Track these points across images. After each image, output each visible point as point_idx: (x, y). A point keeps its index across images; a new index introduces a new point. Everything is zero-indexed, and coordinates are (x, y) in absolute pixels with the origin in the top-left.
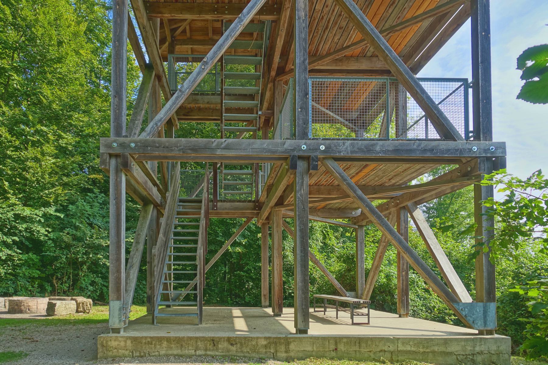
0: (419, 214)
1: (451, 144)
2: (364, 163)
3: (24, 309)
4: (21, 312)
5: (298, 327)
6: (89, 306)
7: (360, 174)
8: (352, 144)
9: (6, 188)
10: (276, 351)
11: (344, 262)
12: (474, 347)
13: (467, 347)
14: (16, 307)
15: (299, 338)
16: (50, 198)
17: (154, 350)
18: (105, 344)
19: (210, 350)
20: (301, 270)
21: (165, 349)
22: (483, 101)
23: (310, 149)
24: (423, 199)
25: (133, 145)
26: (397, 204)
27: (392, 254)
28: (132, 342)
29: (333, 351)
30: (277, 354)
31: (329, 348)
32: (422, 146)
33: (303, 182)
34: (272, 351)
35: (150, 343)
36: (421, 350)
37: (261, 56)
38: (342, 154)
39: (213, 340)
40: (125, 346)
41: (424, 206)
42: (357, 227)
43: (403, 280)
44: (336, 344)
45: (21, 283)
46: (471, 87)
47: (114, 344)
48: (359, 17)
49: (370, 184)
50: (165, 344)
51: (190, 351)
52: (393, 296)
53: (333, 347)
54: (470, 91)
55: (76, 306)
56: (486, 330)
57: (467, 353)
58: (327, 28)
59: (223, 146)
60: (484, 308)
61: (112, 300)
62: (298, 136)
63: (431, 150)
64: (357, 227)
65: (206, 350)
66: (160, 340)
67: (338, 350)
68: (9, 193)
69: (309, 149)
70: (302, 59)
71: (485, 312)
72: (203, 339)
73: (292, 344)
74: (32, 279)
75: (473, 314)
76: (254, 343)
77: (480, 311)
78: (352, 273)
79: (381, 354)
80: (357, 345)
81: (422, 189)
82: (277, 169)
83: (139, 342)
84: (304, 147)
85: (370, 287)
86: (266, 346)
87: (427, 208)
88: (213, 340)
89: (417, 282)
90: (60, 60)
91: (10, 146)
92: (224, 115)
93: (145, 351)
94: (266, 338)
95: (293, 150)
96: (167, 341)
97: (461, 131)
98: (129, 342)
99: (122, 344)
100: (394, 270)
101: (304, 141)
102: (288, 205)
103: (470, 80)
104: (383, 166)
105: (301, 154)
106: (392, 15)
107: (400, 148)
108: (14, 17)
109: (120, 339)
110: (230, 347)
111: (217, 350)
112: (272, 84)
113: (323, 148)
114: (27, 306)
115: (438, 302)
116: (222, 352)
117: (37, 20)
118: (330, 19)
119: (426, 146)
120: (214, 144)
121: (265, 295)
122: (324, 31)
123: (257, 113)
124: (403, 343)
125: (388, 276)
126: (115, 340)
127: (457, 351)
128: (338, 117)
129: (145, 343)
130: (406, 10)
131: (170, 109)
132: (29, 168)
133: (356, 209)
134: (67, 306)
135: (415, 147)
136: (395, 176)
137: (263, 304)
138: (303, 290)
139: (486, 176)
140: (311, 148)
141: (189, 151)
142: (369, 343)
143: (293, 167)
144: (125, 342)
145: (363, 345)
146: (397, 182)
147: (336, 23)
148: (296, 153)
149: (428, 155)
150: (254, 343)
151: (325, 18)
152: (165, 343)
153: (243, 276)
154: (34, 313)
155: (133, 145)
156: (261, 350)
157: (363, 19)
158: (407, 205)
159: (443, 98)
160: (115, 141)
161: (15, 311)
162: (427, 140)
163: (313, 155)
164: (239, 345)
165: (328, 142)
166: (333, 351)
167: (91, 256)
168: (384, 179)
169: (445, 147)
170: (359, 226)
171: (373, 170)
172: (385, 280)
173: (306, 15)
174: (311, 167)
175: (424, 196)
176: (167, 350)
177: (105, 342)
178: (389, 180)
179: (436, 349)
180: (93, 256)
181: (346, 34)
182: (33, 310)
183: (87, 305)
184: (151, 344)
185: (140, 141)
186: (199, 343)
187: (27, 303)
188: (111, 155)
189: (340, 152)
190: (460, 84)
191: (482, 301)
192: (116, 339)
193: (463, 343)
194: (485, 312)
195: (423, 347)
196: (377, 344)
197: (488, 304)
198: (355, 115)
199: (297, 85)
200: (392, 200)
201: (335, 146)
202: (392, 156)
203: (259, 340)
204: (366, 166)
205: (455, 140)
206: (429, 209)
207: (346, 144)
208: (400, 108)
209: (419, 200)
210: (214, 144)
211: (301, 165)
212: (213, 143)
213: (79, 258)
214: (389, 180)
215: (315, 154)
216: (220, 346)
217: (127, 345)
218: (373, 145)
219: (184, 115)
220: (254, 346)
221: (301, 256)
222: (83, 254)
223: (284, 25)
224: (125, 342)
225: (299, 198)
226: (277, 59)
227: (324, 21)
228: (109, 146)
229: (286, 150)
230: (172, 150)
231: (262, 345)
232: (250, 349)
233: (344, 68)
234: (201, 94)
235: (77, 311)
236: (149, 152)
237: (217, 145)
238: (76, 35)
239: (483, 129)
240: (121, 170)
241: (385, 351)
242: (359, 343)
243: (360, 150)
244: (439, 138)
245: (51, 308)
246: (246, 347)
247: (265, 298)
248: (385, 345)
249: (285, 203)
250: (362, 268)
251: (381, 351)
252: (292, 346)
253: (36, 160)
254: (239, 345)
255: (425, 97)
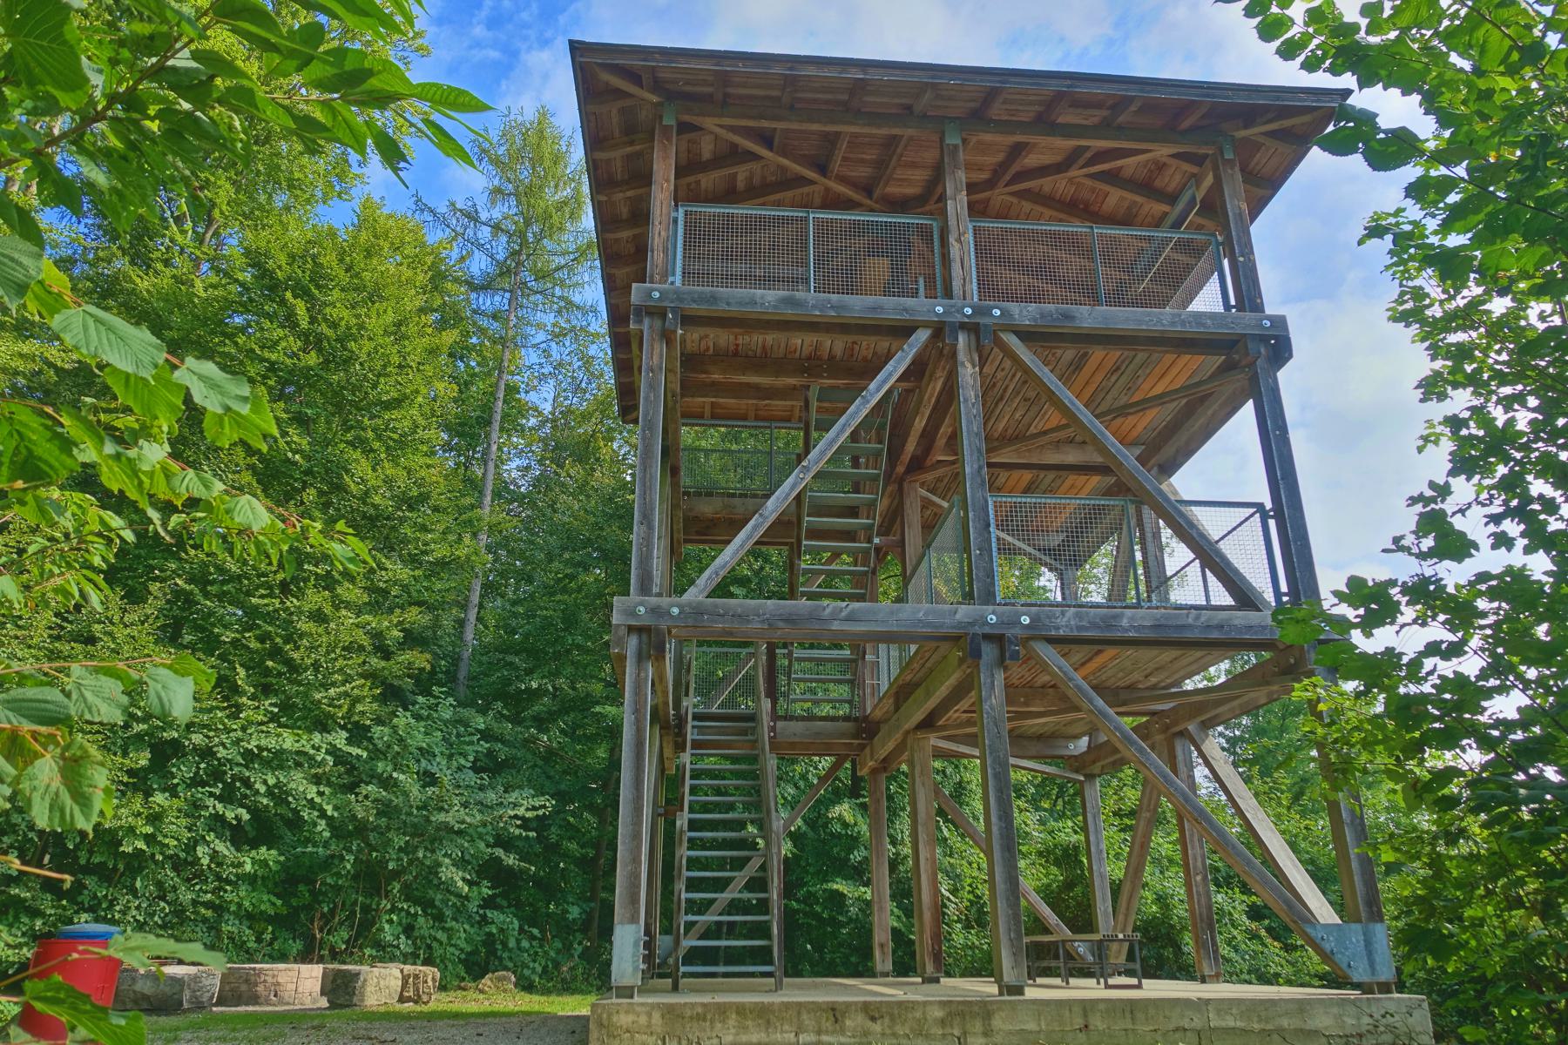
0: (1214, 744)
1: (1251, 617)
2: (1097, 647)
3: (264, 993)
4: (255, 999)
5: (1006, 979)
6: (430, 983)
7: (1088, 665)
8: (1077, 615)
9: (240, 682)
10: (965, 1033)
11: (1057, 863)
12: (1358, 1019)
13: (1345, 1019)
14: (244, 987)
15: (1010, 1001)
16: (340, 707)
17: (709, 1034)
18: (606, 1023)
19: (827, 1032)
20: (1003, 857)
21: (733, 1031)
22: (1295, 543)
23: (1003, 623)
24: (1216, 716)
25: (675, 611)
26: (1167, 728)
27: (1163, 843)
28: (663, 1017)
29: (1080, 1030)
30: (965, 1038)
31: (1072, 1025)
32: (1203, 619)
33: (993, 682)
34: (957, 1032)
35: (700, 1018)
36: (1257, 1026)
37: (880, 442)
38: (1061, 632)
39: (833, 1009)
40: (649, 1026)
41: (1221, 734)
42: (1082, 778)
43: (1199, 894)
44: (1085, 1016)
45: (229, 928)
46: (1272, 517)
47: (624, 1020)
48: (1066, 402)
49: (1108, 684)
50: (733, 1019)
51: (785, 1035)
52: (1180, 949)
53: (1079, 1022)
54: (1272, 523)
55: (400, 983)
56: (1379, 984)
57: (1348, 1032)
58: (1001, 399)
59: (843, 614)
60: (1365, 934)
61: (622, 923)
62: (979, 598)
63: (1220, 627)
64: (1082, 778)
65: (819, 1033)
66: (722, 1010)
67: (1091, 1027)
68: (243, 693)
69: (1000, 623)
70: (976, 466)
71: (1368, 944)
72: (814, 1008)
73: (997, 1016)
74: (251, 918)
75: (1346, 949)
76: (918, 1015)
77: (1358, 941)
78: (1078, 890)
79: (1177, 1035)
80: (1128, 1015)
81: (1213, 696)
82: (927, 655)
83: (678, 1016)
84: (992, 619)
85: (1126, 920)
86: (943, 1022)
87: (1228, 741)
88: (833, 1009)
89: (1230, 914)
90: (397, 403)
91: (258, 587)
92: (804, 543)
93: (690, 1036)
94: (943, 1004)
95: (972, 624)
96: (738, 1013)
97: (1269, 596)
98: (656, 1016)
99: (643, 1020)
100: (1174, 885)
101: (991, 608)
102: (944, 728)
103: (1269, 505)
104: (1130, 652)
105: (987, 630)
106: (1117, 386)
107: (1163, 622)
108: (313, 320)
109: (638, 1009)
110: (869, 1023)
111: (842, 1032)
112: (896, 486)
113: (1025, 620)
114: (273, 984)
115: (1284, 962)
116: (854, 1037)
117: (361, 327)
118: (1007, 387)
119: (1209, 619)
120: (828, 611)
121: (882, 946)
122: (997, 404)
123: (869, 541)
124: (1218, 1012)
125: (1161, 899)
126: (627, 1012)
127: (1326, 1028)
128: (1019, 544)
129: (691, 1018)
130: (1141, 380)
131: (742, 546)
132: (301, 636)
133: (1077, 737)
134: (382, 982)
135: (1190, 621)
136: (1157, 669)
137: (879, 968)
138: (1008, 899)
139: (1297, 685)
140: (1006, 620)
141: (781, 624)
142: (1152, 1012)
143: (976, 654)
144: (649, 1015)
145: (1140, 1016)
146: (1162, 681)
147: (1018, 393)
148: (978, 630)
149: (1215, 635)
150: (918, 1015)
151: (999, 385)
152: (734, 1016)
153: (797, 911)
154: (288, 1004)
155: (675, 611)
156: (932, 1031)
157: (1074, 404)
158: (1186, 729)
159: (1229, 537)
160: (641, 604)
161: (240, 997)
162: (1208, 607)
163: (1009, 633)
164: (887, 1020)
165: (1034, 609)
166: (1080, 1030)
167: (420, 855)
168: (1136, 676)
169: (1243, 622)
170: (1085, 776)
171: (1114, 658)
172: (1154, 908)
173: (977, 396)
174: (1007, 655)
175: (1220, 710)
176: (737, 1034)
177: (605, 1016)
178: (1146, 677)
179: (1285, 1023)
180: (425, 856)
181: (1035, 409)
182: (286, 995)
183: (426, 982)
184: (704, 1020)
185: (689, 604)
186: (805, 1016)
187: (274, 976)
188: (631, 629)
189: (1058, 628)
190: (1252, 510)
191: (1359, 921)
192: (630, 1009)
193: (1335, 1010)
194: (1368, 944)
195: (1260, 1021)
196: (1167, 1013)
197: (1371, 925)
198: (1055, 540)
199: (970, 509)
200: (1155, 718)
201: (1048, 617)
202: (1151, 635)
203: (928, 1008)
204: (1099, 652)
205: (1259, 610)
206: (1233, 742)
207: (1068, 615)
208: (1149, 536)
209: (1209, 719)
210: (828, 611)
211: (989, 652)
212: (824, 609)
213: (387, 861)
214: (1146, 677)
215: (1013, 631)
216: (848, 1023)
217: (653, 1021)
218: (1115, 617)
219: (698, 533)
220: (919, 1020)
221: (1000, 828)
222: (400, 850)
223: (930, 399)
224: (649, 1015)
225: (988, 713)
226: (911, 447)
227: (996, 390)
228: (632, 613)
229: (960, 623)
230: (748, 621)
231: (935, 1020)
232: (912, 1030)
233: (1035, 461)
234: (741, 496)
235: (402, 1000)
236: (706, 624)
237: (832, 613)
238: (433, 352)
239: (1305, 592)
240: (649, 657)
241: (1185, 1030)
242: (1132, 1012)
243: (1094, 625)
244: (1248, 410)
245: (340, 990)
246: (903, 1024)
247: (883, 953)
248: (1183, 1016)
249: (940, 723)
250: (1102, 876)
251: (1177, 1029)
252: (997, 1022)
253: (319, 617)
254: (887, 1020)
255: (1195, 535)
